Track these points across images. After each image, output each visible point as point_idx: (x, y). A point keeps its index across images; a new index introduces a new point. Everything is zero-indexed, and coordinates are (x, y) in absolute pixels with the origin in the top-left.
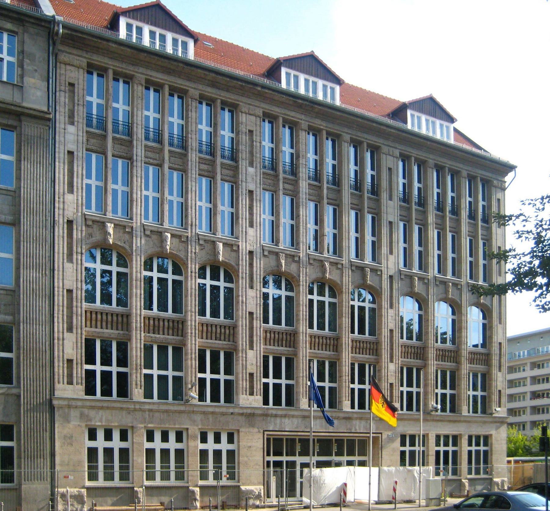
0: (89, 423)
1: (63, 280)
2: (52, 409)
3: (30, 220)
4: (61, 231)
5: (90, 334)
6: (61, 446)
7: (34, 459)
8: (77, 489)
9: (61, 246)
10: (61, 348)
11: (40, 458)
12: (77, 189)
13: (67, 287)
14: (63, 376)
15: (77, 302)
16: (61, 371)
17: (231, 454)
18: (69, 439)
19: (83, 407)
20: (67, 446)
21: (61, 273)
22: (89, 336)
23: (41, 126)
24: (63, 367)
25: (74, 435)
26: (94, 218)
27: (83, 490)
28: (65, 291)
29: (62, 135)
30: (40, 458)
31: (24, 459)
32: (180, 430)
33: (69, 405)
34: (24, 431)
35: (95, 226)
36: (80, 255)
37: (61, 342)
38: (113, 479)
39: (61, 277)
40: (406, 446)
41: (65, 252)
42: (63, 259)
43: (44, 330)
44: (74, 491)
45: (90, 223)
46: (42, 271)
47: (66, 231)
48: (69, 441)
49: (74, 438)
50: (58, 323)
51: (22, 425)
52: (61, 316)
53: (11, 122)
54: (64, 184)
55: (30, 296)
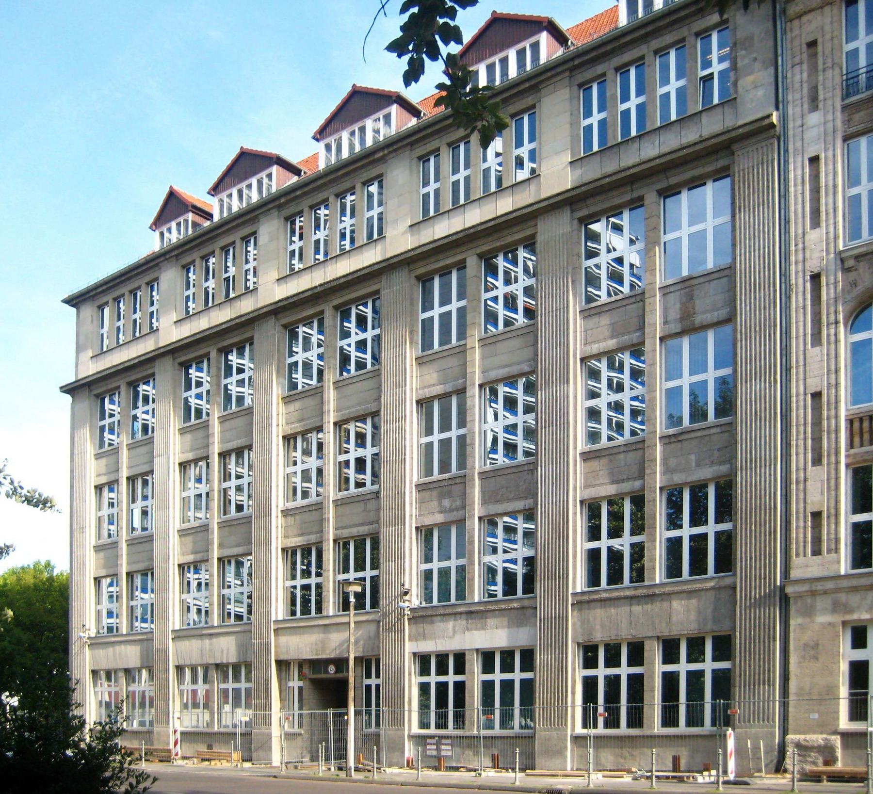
0: (848, 617)
1: (805, 379)
2: (785, 601)
3: (750, 303)
4: (801, 297)
5: (859, 459)
6: (799, 663)
7: (754, 686)
8: (825, 736)
9: (801, 324)
10: (801, 496)
11: (764, 684)
12: (827, 214)
13: (812, 389)
14: (805, 542)
15: (829, 410)
16: (801, 536)
17: (528, 687)
18: (813, 650)
19: (838, 590)
20: (809, 661)
21: (801, 369)
22: (858, 462)
23: (763, 144)
24: (805, 528)
25: (820, 642)
26: (856, 252)
27: (833, 737)
28: (809, 396)
29: (799, 138)
30: (764, 684)
31: (740, 687)
32: (860, 624)
33: (811, 591)
34: (740, 643)
35: (861, 264)
36: (833, 326)
37: (801, 487)
38: (493, 728)
39: (801, 377)
40: (429, 675)
41: (809, 331)
42: (805, 344)
43: (772, 473)
44: (818, 739)
45: (851, 263)
46: (770, 377)
47: (809, 296)
48: (812, 652)
49: (820, 647)
50: (797, 455)
51: (738, 634)
52: (801, 442)
53: (721, 163)
54: (803, 217)
55: (751, 425)
